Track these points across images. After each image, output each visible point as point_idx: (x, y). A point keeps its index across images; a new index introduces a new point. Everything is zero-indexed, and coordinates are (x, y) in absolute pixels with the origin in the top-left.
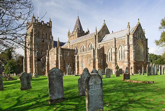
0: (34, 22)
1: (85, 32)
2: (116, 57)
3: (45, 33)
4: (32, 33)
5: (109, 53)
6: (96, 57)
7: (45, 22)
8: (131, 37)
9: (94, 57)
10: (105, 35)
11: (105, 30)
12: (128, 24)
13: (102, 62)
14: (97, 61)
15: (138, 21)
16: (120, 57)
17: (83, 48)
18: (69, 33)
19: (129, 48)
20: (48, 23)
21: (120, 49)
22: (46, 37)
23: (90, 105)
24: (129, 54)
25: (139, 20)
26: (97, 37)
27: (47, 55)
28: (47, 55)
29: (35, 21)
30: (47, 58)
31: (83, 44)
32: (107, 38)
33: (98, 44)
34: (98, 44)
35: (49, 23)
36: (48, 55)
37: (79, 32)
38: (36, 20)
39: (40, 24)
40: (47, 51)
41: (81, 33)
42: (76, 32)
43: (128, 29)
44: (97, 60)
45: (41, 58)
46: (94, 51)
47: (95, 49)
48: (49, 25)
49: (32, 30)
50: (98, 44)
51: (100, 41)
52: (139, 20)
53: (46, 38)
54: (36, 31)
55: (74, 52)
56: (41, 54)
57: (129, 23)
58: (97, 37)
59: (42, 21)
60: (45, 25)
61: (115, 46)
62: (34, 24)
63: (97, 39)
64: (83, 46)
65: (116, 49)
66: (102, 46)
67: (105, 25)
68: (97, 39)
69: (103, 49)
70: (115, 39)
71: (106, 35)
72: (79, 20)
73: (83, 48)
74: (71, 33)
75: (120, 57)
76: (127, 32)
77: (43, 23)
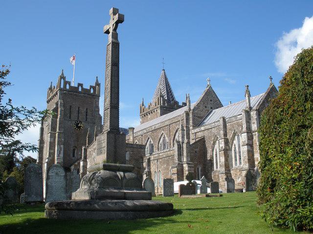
0: (62, 87)
1: (180, 104)
2: (226, 160)
3: (85, 110)
4: (56, 110)
5: (215, 151)
6: (185, 160)
7: (86, 86)
8: (254, 114)
9: (180, 159)
10: (211, 111)
11: (211, 101)
12: (246, 88)
13: (201, 171)
14: (187, 169)
15: (270, 82)
16: (236, 160)
17: (164, 140)
18: (143, 105)
19: (250, 138)
20: (91, 87)
21: (235, 142)
22: (85, 117)
23: (48, 195)
24: (251, 153)
25: (271, 79)
26: (191, 116)
27: (83, 158)
28: (83, 158)
29: (65, 86)
30: (82, 163)
31: (163, 132)
32: (216, 116)
33: (193, 131)
34: (192, 131)
35: (94, 88)
36: (85, 158)
37: (164, 103)
38: (66, 83)
39: (74, 90)
40: (83, 148)
41: (169, 104)
42: (157, 103)
43: (247, 98)
44: (186, 166)
45: (71, 166)
46: (180, 148)
47: (183, 143)
48: (95, 91)
49: (57, 104)
50: (193, 131)
51: (197, 124)
52: (271, 79)
53: (86, 120)
54: (64, 105)
55: (142, 150)
56: (74, 156)
57: (248, 86)
58: (191, 116)
59: (80, 85)
60: (86, 91)
61: (225, 135)
62: (61, 90)
63: (191, 122)
64: (164, 137)
65: (227, 142)
66: (200, 135)
67: (211, 90)
68: (191, 122)
69: (202, 141)
70: (224, 119)
71: (214, 111)
72: (166, 79)
73: (164, 140)
74: (147, 107)
75: (236, 160)
76: (244, 105)
77: (82, 87)
